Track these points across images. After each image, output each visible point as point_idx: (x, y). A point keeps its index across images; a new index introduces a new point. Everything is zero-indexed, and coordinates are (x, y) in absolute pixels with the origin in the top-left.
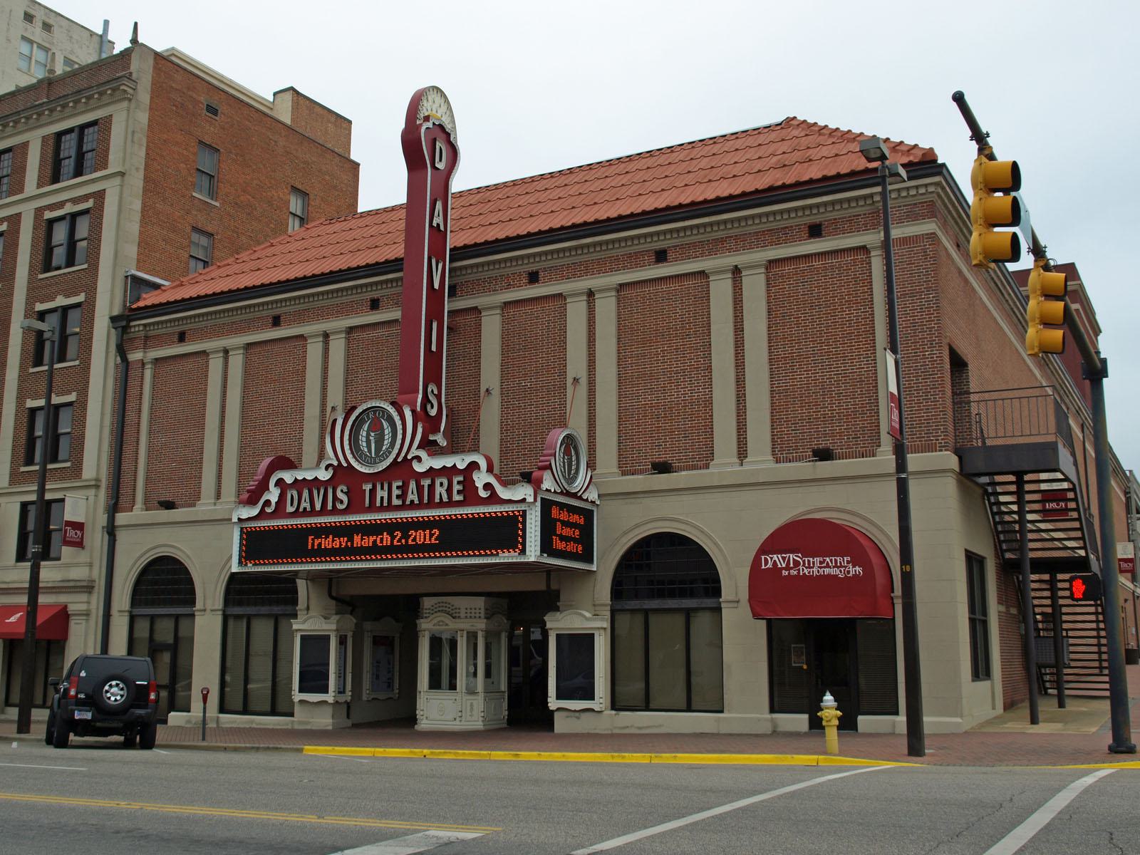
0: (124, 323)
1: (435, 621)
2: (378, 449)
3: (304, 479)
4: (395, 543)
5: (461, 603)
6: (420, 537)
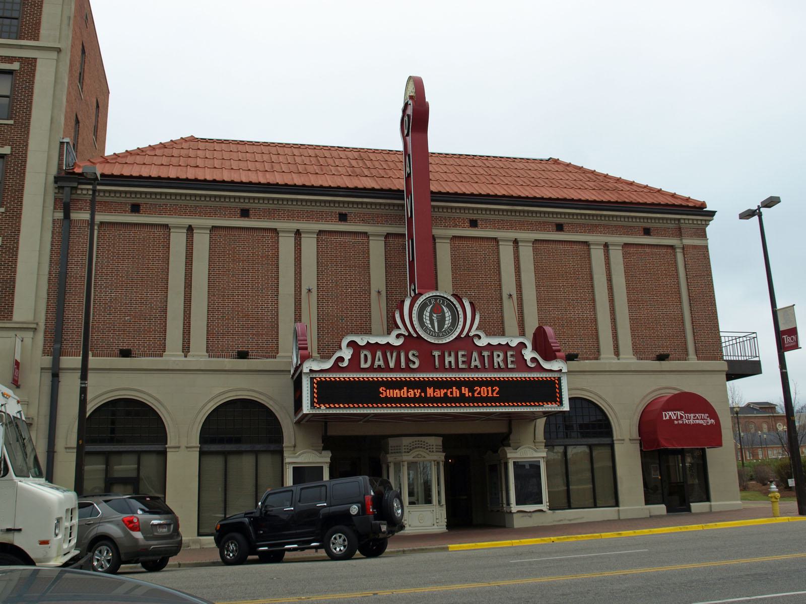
0: (75, 185)
1: (414, 455)
3: (489, 344)
4: (476, 395)
6: (484, 391)
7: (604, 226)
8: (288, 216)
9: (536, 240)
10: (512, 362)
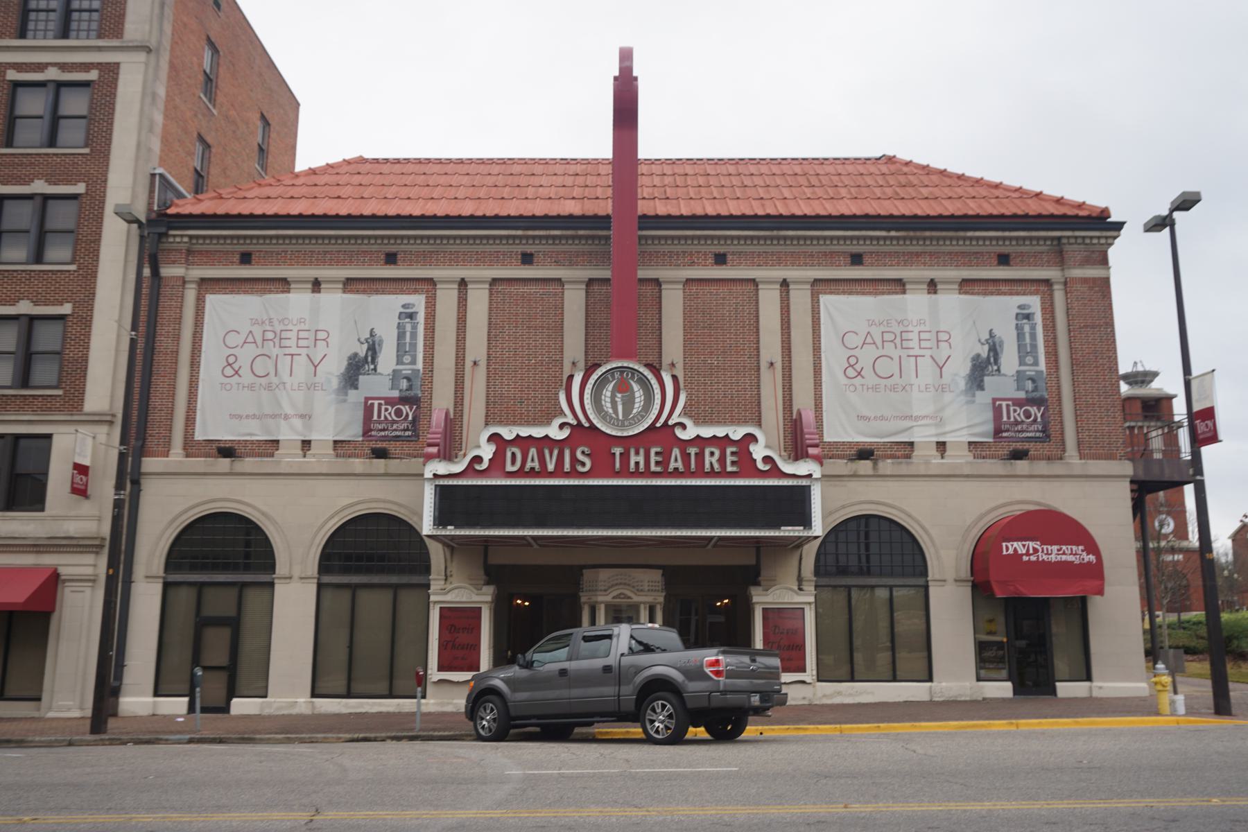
0: (163, 230)
1: (615, 593)
2: (627, 411)
5: (639, 574)
7: (931, 254)
8: (450, 260)
9: (816, 281)
10: (657, 463)
